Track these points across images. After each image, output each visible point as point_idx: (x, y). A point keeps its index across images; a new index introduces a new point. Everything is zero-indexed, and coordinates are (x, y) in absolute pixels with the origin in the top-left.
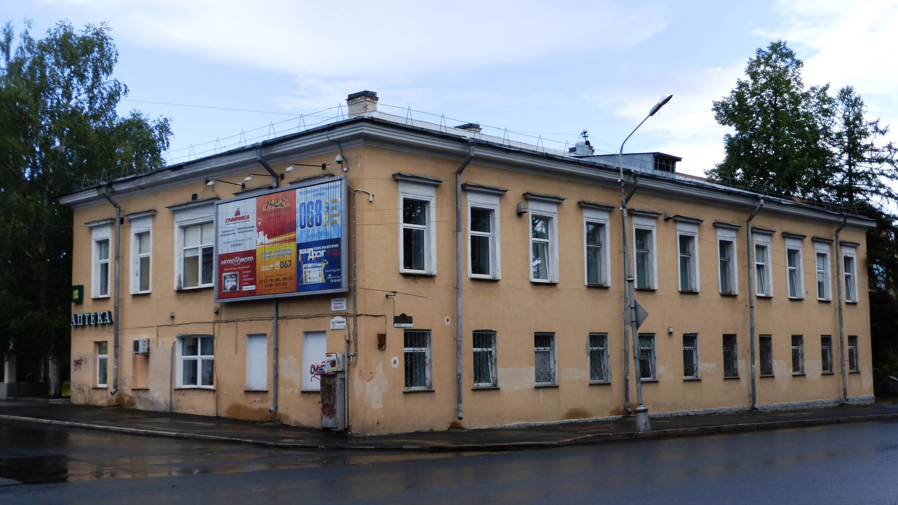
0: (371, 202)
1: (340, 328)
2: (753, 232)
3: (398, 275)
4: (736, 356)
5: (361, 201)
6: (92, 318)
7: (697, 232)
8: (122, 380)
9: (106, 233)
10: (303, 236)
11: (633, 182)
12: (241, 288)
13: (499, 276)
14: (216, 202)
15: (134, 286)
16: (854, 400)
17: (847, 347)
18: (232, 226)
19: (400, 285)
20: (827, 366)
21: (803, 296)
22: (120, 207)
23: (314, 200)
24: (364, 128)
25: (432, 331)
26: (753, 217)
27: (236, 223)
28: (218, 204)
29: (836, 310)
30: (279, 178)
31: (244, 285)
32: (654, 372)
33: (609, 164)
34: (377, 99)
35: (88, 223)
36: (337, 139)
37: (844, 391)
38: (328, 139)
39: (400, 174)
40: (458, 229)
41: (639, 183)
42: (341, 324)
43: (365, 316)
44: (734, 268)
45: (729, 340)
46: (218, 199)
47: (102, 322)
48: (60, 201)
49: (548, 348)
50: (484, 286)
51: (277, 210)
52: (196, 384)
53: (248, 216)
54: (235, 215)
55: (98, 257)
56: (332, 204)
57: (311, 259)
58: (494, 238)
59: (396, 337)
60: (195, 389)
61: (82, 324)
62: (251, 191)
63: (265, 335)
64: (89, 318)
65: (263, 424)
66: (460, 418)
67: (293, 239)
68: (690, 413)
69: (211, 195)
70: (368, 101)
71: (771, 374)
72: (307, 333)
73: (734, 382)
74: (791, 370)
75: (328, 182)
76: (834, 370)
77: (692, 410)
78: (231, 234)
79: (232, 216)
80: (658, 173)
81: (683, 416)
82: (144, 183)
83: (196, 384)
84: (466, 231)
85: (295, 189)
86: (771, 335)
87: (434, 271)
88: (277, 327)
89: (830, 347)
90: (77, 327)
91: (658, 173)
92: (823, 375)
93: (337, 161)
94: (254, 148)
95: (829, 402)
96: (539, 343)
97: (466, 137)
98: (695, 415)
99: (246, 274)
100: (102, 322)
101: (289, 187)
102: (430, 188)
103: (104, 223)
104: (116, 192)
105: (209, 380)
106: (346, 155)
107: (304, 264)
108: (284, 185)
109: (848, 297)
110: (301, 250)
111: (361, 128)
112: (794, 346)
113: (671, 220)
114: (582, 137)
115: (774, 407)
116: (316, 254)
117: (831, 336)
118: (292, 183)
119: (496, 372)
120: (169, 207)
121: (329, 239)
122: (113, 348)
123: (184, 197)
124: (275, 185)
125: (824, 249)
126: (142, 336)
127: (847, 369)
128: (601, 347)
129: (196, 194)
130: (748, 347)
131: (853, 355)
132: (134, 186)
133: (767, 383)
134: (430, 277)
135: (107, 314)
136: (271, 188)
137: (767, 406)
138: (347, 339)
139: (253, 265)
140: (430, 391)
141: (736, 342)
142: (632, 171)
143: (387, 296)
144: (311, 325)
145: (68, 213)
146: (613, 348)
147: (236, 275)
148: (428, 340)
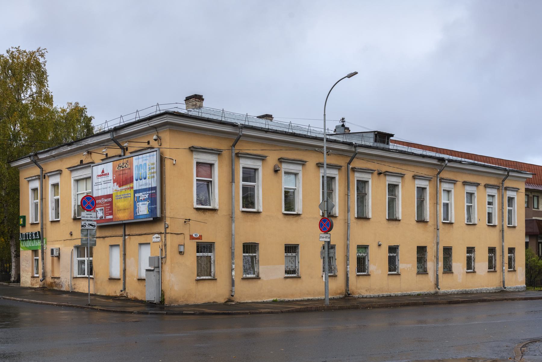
0: (174, 164)
1: (158, 241)
2: (441, 182)
3: (193, 209)
4: (426, 261)
5: (168, 163)
6: (30, 235)
7: (401, 181)
8: (46, 272)
9: (36, 184)
10: (136, 185)
11: (354, 150)
12: (105, 217)
13: (261, 210)
14: (92, 165)
15: (51, 215)
16: (510, 288)
17: (507, 255)
18: (100, 180)
19: (193, 215)
20: (491, 266)
21: (476, 222)
22: (42, 169)
23: (143, 163)
24: (168, 118)
25: (215, 243)
26: (442, 171)
27: (102, 178)
28: (93, 166)
29: (500, 230)
30: (125, 150)
31: (107, 216)
32: (368, 270)
33: (337, 139)
34: (203, 100)
35: (26, 178)
36: (153, 125)
37: (503, 282)
38: (148, 126)
39: (193, 147)
40: (233, 181)
41: (358, 151)
42: (158, 239)
43: (170, 234)
44: (426, 204)
45: (421, 250)
46: (93, 163)
47: (35, 238)
48: (11, 165)
49: (294, 254)
50: (250, 216)
51: (124, 170)
52: (84, 275)
53: (108, 173)
54: (102, 173)
55: (33, 199)
56: (152, 166)
57: (141, 200)
58: (258, 186)
59: (191, 247)
60: (83, 277)
61: (25, 239)
62: (110, 158)
63: (118, 245)
64: (29, 235)
65: (116, 298)
66: (233, 296)
67: (132, 187)
68: (392, 295)
69: (90, 160)
70: (197, 101)
71: (451, 271)
72: (141, 244)
73: (424, 276)
74: (488, 269)
75: (150, 152)
76: (497, 269)
77: (393, 293)
78: (100, 184)
79: (100, 173)
80: (376, 145)
81: (387, 296)
82: (54, 154)
83: (84, 275)
84: (239, 182)
85: (133, 157)
86: (452, 247)
87: (217, 207)
88: (125, 241)
89: (495, 255)
90: (23, 240)
91: (376, 145)
92: (488, 272)
93: (154, 139)
94: (109, 132)
95: (492, 289)
96: (288, 251)
97: (237, 123)
98: (395, 296)
99: (108, 209)
100: (35, 238)
101: (129, 155)
102: (214, 155)
103: (34, 178)
104: (40, 159)
105: (91, 272)
106: (160, 135)
107: (137, 202)
108: (128, 155)
109: (510, 222)
110: (136, 194)
111: (166, 118)
112: (510, 254)
113: (382, 174)
114: (341, 122)
115: (452, 292)
116: (144, 197)
117: (495, 247)
118: (131, 153)
119: (258, 268)
120: (68, 168)
121: (148, 188)
122: (41, 253)
123: (75, 161)
124: (122, 154)
125: (494, 192)
126: (56, 246)
127: (506, 267)
128: (395, 254)
129: (82, 160)
130: (434, 254)
131: (511, 261)
132: (49, 155)
133: (448, 277)
134: (214, 210)
135: (38, 233)
136: (120, 156)
137: (447, 291)
138: (161, 247)
139: (111, 203)
140: (214, 279)
141: (426, 251)
142: (354, 143)
143: (185, 222)
144: (142, 239)
145: (16, 173)
146: (430, 254)
147: (103, 209)
148: (257, 249)
